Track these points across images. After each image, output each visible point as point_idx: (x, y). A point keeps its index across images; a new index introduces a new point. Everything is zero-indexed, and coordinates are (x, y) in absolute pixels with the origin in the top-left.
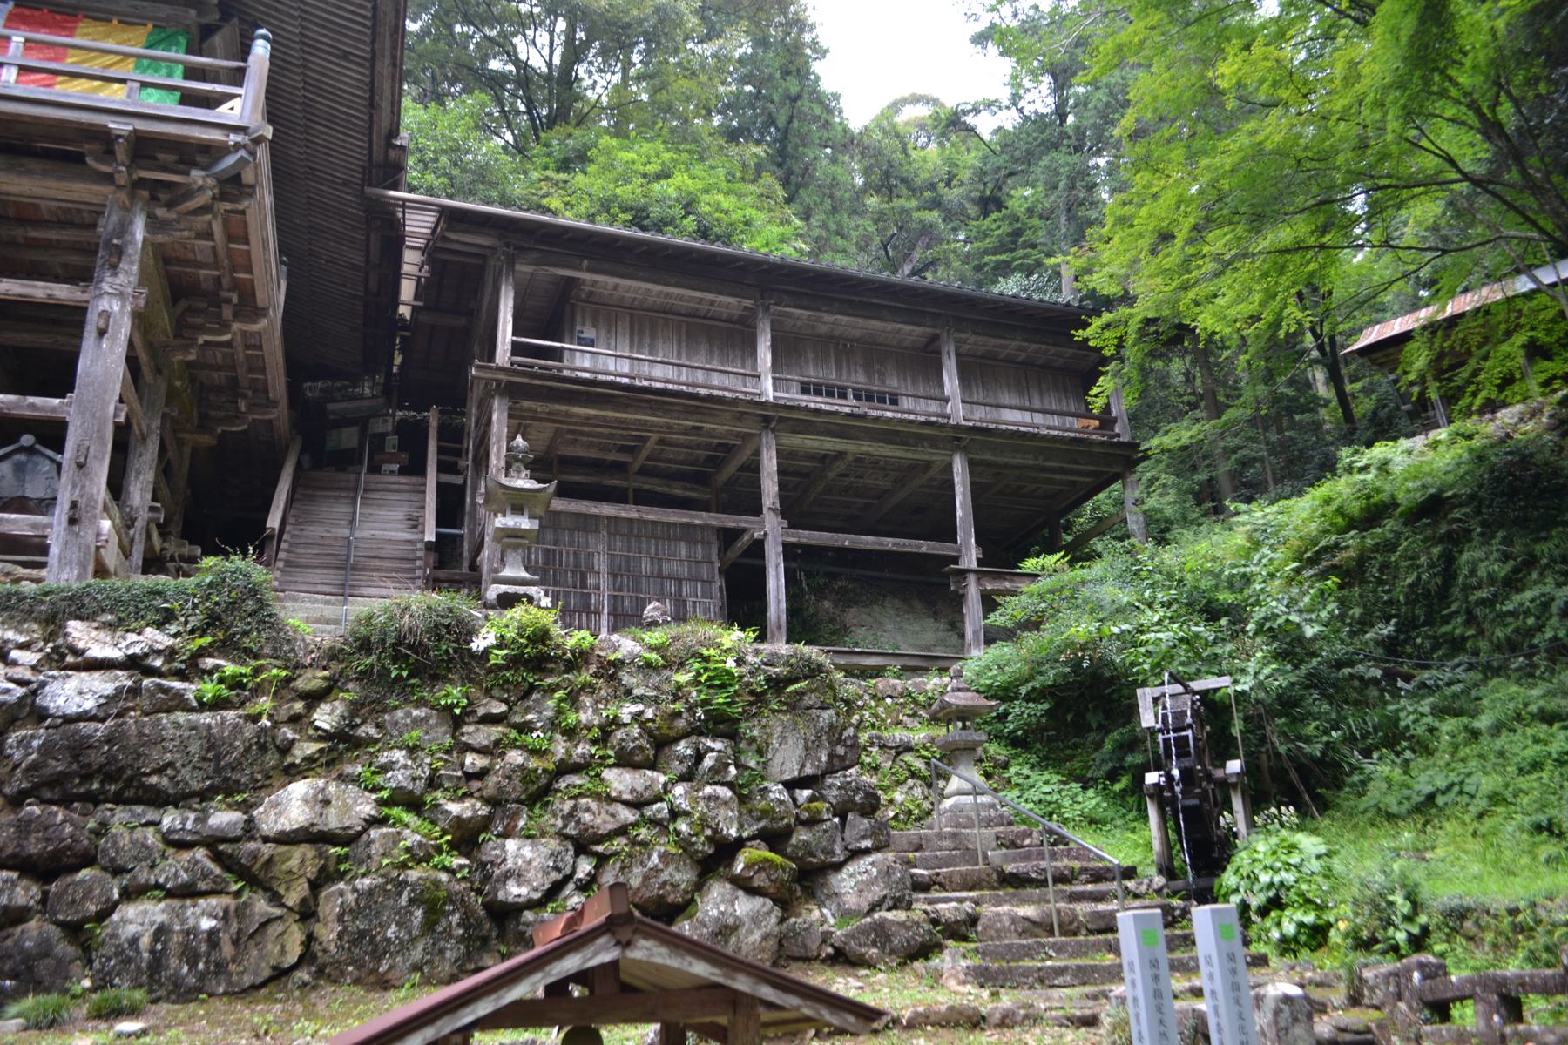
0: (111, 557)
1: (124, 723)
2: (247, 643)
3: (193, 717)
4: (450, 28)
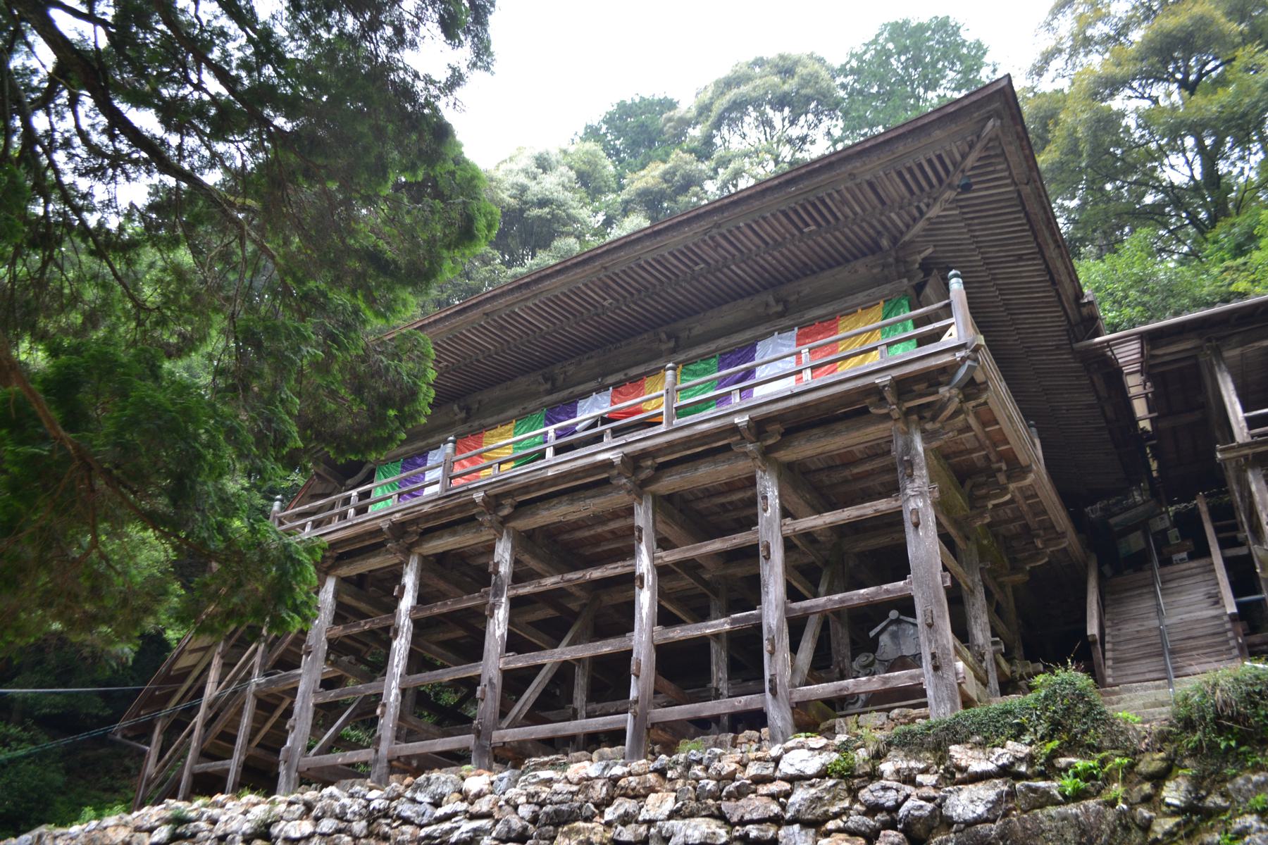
0: (972, 689)
1: (1010, 821)
2: (1088, 740)
3: (1062, 809)
4: (1102, 189)
